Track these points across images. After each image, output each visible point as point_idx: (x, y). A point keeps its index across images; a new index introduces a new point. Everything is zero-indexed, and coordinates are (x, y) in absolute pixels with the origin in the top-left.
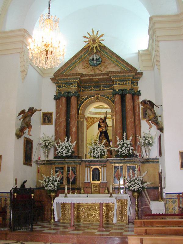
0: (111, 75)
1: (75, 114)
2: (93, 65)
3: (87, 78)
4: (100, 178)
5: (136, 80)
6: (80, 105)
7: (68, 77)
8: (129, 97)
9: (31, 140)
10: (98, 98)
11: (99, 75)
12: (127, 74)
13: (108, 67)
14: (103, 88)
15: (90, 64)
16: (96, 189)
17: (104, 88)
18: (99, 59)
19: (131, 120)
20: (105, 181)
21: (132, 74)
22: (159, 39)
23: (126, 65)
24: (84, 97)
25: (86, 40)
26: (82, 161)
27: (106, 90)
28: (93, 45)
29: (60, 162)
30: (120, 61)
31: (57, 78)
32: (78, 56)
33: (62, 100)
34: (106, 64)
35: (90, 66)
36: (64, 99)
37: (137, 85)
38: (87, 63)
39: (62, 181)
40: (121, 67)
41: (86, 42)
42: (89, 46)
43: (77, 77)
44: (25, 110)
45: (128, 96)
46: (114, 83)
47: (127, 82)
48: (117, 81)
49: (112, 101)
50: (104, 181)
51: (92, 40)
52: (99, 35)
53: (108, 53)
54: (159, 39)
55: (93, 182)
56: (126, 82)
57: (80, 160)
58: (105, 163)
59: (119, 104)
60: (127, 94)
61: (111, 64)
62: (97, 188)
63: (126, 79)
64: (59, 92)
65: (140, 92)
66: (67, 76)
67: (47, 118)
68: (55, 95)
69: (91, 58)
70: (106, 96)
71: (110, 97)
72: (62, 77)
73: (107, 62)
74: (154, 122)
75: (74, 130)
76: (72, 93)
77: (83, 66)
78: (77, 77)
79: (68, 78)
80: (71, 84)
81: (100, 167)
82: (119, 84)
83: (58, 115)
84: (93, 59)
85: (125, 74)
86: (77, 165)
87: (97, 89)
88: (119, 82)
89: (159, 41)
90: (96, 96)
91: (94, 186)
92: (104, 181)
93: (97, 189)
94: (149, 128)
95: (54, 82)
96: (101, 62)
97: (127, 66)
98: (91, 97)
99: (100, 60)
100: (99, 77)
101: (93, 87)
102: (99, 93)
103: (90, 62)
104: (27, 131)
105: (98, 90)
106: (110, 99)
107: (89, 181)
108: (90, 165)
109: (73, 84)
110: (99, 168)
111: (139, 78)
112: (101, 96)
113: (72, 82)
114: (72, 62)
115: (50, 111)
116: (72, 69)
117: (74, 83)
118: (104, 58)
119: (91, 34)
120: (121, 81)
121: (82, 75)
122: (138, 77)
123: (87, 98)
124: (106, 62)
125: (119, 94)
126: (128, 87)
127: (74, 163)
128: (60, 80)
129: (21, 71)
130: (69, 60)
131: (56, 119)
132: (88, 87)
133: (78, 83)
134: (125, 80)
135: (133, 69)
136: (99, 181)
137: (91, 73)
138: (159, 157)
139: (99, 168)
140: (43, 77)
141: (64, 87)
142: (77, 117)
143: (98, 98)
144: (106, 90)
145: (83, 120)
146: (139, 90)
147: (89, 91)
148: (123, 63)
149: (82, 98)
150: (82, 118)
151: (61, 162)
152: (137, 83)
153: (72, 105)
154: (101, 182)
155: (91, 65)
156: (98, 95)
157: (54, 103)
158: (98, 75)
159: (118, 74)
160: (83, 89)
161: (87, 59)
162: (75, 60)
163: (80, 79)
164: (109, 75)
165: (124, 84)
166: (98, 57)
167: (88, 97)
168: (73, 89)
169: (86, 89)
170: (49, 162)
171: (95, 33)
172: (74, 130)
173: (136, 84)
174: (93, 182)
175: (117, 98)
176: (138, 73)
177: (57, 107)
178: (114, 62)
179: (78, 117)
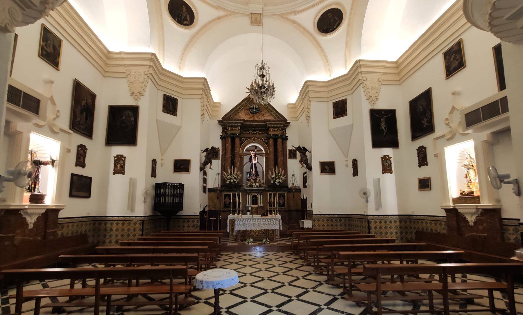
0: (268, 122)
2: (253, 113)
7: (234, 121)
8: (280, 141)
10: (254, 140)
13: (264, 115)
15: (250, 112)
18: (258, 108)
19: (281, 159)
20: (262, 205)
21: (283, 123)
24: (243, 138)
27: (261, 134)
30: (274, 112)
31: (224, 121)
34: (263, 113)
36: (230, 139)
37: (285, 132)
38: (248, 111)
39: (229, 205)
43: (241, 122)
44: (208, 148)
45: (279, 140)
46: (269, 129)
50: (261, 205)
54: (311, 99)
58: (261, 192)
60: (278, 139)
61: (266, 113)
66: (233, 121)
68: (221, 135)
69: (252, 107)
70: (261, 139)
74: (306, 163)
76: (236, 134)
78: (241, 122)
85: (278, 123)
87: (254, 133)
89: (311, 101)
90: (253, 138)
95: (220, 125)
96: (259, 110)
99: (259, 109)
100: (258, 123)
103: (251, 110)
110: (257, 195)
111: (287, 126)
112: (257, 138)
113: (236, 125)
116: (236, 114)
117: (238, 127)
118: (261, 107)
120: (274, 128)
121: (245, 121)
124: (263, 111)
125: (273, 138)
126: (279, 132)
128: (227, 123)
129: (131, 95)
131: (222, 155)
135: (285, 120)
137: (251, 119)
138: (301, 187)
139: (257, 195)
140: (211, 119)
144: (261, 134)
147: (248, 133)
148: (276, 113)
149: (242, 139)
152: (285, 130)
153: (236, 144)
155: (251, 113)
159: (273, 123)
162: (239, 107)
163: (242, 123)
165: (276, 130)
166: (257, 107)
167: (247, 138)
168: (237, 131)
175: (271, 141)
178: (269, 112)
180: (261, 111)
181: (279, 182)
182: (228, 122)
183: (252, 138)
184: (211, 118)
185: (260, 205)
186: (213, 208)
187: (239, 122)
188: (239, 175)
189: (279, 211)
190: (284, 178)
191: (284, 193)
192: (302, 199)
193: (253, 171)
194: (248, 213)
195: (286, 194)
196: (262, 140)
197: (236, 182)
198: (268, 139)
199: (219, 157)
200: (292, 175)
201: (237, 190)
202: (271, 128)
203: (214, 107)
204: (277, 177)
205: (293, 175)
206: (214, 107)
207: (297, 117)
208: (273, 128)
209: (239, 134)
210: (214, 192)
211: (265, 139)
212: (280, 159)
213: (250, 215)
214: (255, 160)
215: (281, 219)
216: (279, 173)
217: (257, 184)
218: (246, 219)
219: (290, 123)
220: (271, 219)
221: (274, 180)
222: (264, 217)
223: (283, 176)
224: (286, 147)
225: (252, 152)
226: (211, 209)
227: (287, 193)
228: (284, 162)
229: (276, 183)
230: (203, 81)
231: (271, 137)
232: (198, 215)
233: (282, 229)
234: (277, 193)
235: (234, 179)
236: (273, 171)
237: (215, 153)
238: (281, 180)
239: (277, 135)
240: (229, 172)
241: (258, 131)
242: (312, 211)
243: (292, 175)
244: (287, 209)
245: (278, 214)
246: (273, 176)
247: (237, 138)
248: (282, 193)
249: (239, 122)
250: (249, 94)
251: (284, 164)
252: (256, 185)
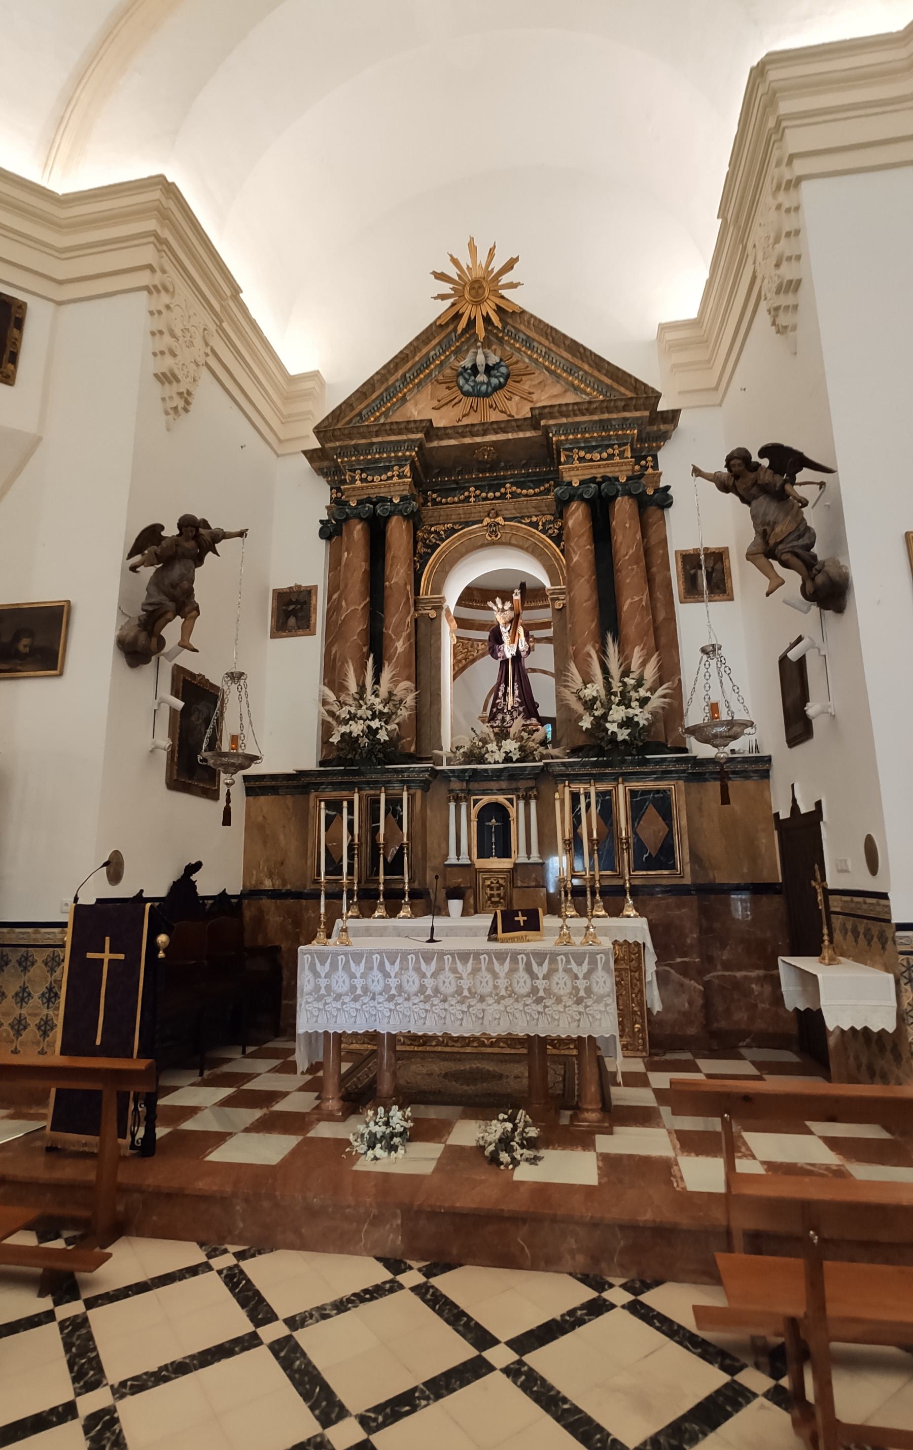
0: (551, 422)
1: (406, 585)
2: (477, 394)
3: (453, 442)
4: (514, 847)
5: (650, 448)
6: (424, 559)
9: (211, 684)
11: (498, 427)
12: (615, 416)
14: (514, 488)
15: (461, 388)
16: (495, 892)
17: (519, 491)
18: (497, 366)
19: (637, 599)
21: (637, 414)
22: (800, 167)
23: (611, 378)
25: (446, 288)
26: (434, 773)
27: (527, 496)
28: (474, 307)
29: (340, 779)
30: (586, 367)
32: (415, 355)
33: (350, 533)
34: (526, 387)
35: (462, 396)
36: (359, 527)
37: (655, 467)
38: (448, 388)
40: (588, 394)
41: (443, 297)
42: (457, 317)
45: (623, 508)
47: (617, 452)
48: (576, 450)
49: (550, 537)
50: (529, 858)
51: (472, 288)
52: (497, 265)
53: (534, 340)
55: (481, 863)
56: (610, 451)
57: (426, 770)
58: (531, 783)
59: (585, 538)
60: (616, 496)
62: (498, 889)
63: (609, 437)
64: (338, 503)
65: (670, 492)
69: (467, 363)
71: (544, 525)
72: (352, 439)
73: (531, 380)
75: (400, 650)
76: (391, 501)
77: (432, 399)
79: (373, 444)
80: (388, 468)
81: (511, 801)
82: (581, 459)
83: (335, 596)
84: (474, 370)
85: (606, 416)
86: (412, 791)
87: (491, 495)
88: (582, 454)
90: (487, 521)
91: (488, 883)
92: (529, 858)
93: (499, 895)
94: (767, 589)
95: (320, 471)
96: (507, 377)
97: (615, 385)
98: (467, 524)
99: (503, 370)
100: (501, 437)
101: (477, 488)
102: (498, 507)
103: (461, 381)
104: (172, 631)
106: (544, 531)
107: (464, 860)
108: (470, 792)
109: (396, 468)
110: (507, 803)
111: (664, 437)
112: (505, 519)
113: (389, 459)
114: (390, 383)
115: (305, 583)
117: (401, 466)
118: (517, 362)
119: (465, 260)
120: (590, 449)
121: (430, 430)
122: (660, 430)
123: (453, 531)
124: (524, 378)
129: (156, 375)
130: (377, 373)
132: (455, 489)
133: (413, 469)
134: (606, 443)
136: (510, 857)
137: (465, 421)
139: (507, 803)
140: (278, 456)
142: (411, 601)
143: (493, 529)
144: (527, 496)
145: (439, 617)
146: (662, 485)
147: (460, 501)
148: (596, 373)
149: (431, 533)
150: (434, 608)
151: (346, 779)
152: (655, 458)
153: (390, 548)
154: (515, 864)
155: (467, 394)
156: (497, 516)
157: (321, 547)
158: (495, 426)
160: (434, 496)
161: (448, 372)
162: (400, 373)
164: (542, 423)
165: (601, 459)
166: (494, 359)
167: (456, 527)
169: (447, 498)
170: (295, 783)
171: (482, 258)
172: (400, 650)
173: (650, 464)
174: (481, 863)
175: (577, 516)
176: (662, 412)
177: (334, 564)
178: (558, 377)
179: (415, 603)
180: (518, 379)
181: (628, 722)
182: (347, 447)
183: (481, 522)
184: (279, 452)
185: (522, 859)
186: (270, 875)
187: (404, 437)
188: (401, 701)
189: (635, 891)
190: (656, 702)
191: (662, 785)
192: (785, 814)
193: (511, 695)
194: (455, 906)
195: (675, 788)
196: (534, 525)
197: (383, 736)
198: (561, 507)
199: (312, 622)
200: (704, 650)
201: (385, 777)
202: (571, 450)
203: (288, 398)
204: (615, 694)
205: (709, 651)
206: (288, 398)
207: (714, 385)
208: (580, 448)
209: (403, 499)
210: (277, 794)
211: (551, 522)
212: (629, 601)
213: (465, 913)
214: (513, 639)
215: (649, 944)
216: (626, 673)
217: (511, 745)
218: (371, 953)
219: (672, 416)
220: (553, 956)
221: (597, 713)
222: (512, 940)
223: (653, 690)
224: (664, 542)
225: (500, 606)
226: (262, 883)
227: (681, 783)
228: (654, 620)
229: (612, 727)
230: (157, 203)
231: (574, 496)
232: (63, 925)
233: (657, 1007)
234: (621, 787)
235: (373, 719)
236: (589, 665)
237: (291, 607)
238: (638, 711)
239: (605, 478)
240: (353, 688)
241: (512, 484)
242: (884, 896)
243: (704, 650)
244: (688, 881)
245: (633, 913)
246: (594, 690)
247: (394, 519)
248: (650, 785)
249: (404, 437)
250: (452, 300)
251: (656, 630)
252: (500, 748)
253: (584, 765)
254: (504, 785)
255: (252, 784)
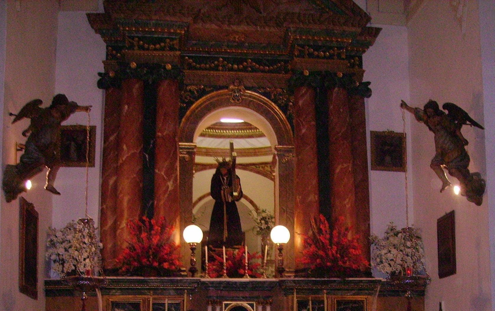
21: (354, 29)
27: (263, 71)
67: (73, 144)
68: (103, 71)
81: (252, 306)
82: (310, 55)
83: (112, 138)
105: (239, 70)
127: (176, 290)
141: (136, 48)
146: (365, 80)
151: (132, 286)
152: (360, 59)
212: (340, 167)
253: (307, 282)
254: (247, 294)
255: (51, 287)
